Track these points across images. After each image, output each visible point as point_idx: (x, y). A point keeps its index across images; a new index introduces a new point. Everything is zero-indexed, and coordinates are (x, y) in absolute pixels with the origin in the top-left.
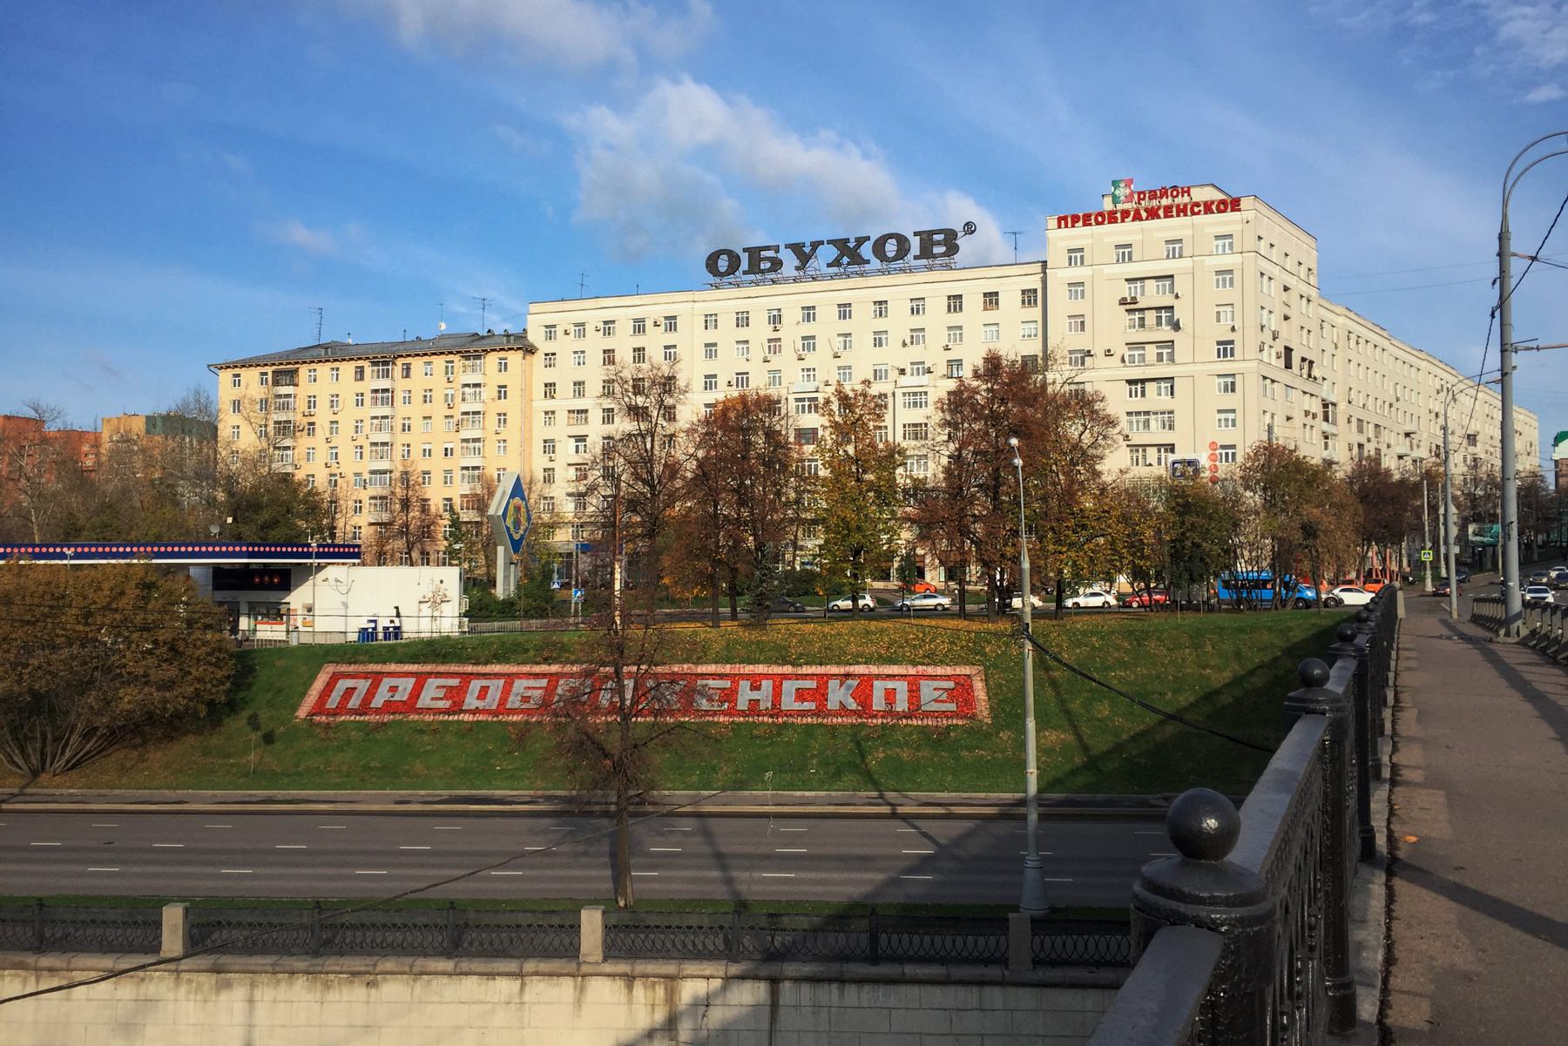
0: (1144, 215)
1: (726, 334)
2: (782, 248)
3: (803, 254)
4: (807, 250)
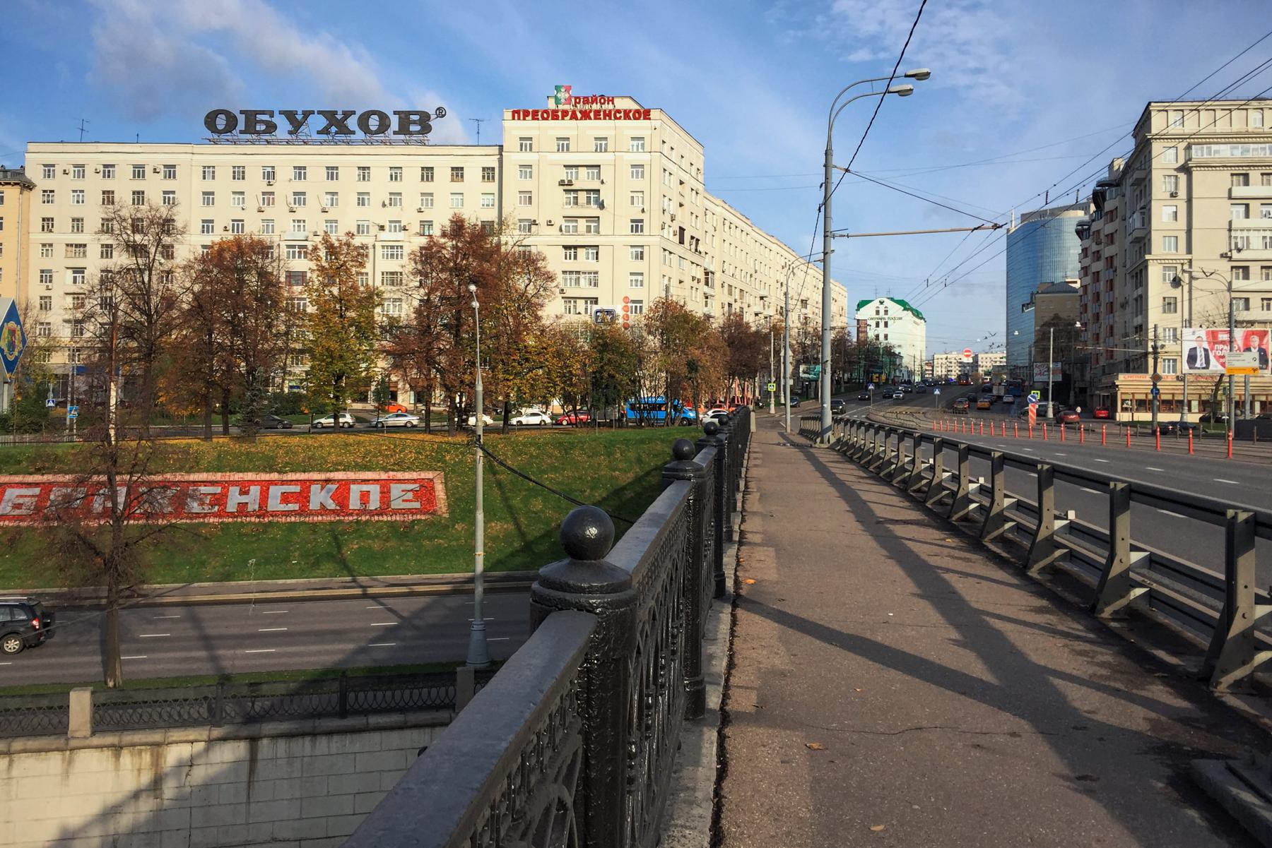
0: (579, 115)
1: (223, 185)
2: (276, 114)
4: (299, 117)
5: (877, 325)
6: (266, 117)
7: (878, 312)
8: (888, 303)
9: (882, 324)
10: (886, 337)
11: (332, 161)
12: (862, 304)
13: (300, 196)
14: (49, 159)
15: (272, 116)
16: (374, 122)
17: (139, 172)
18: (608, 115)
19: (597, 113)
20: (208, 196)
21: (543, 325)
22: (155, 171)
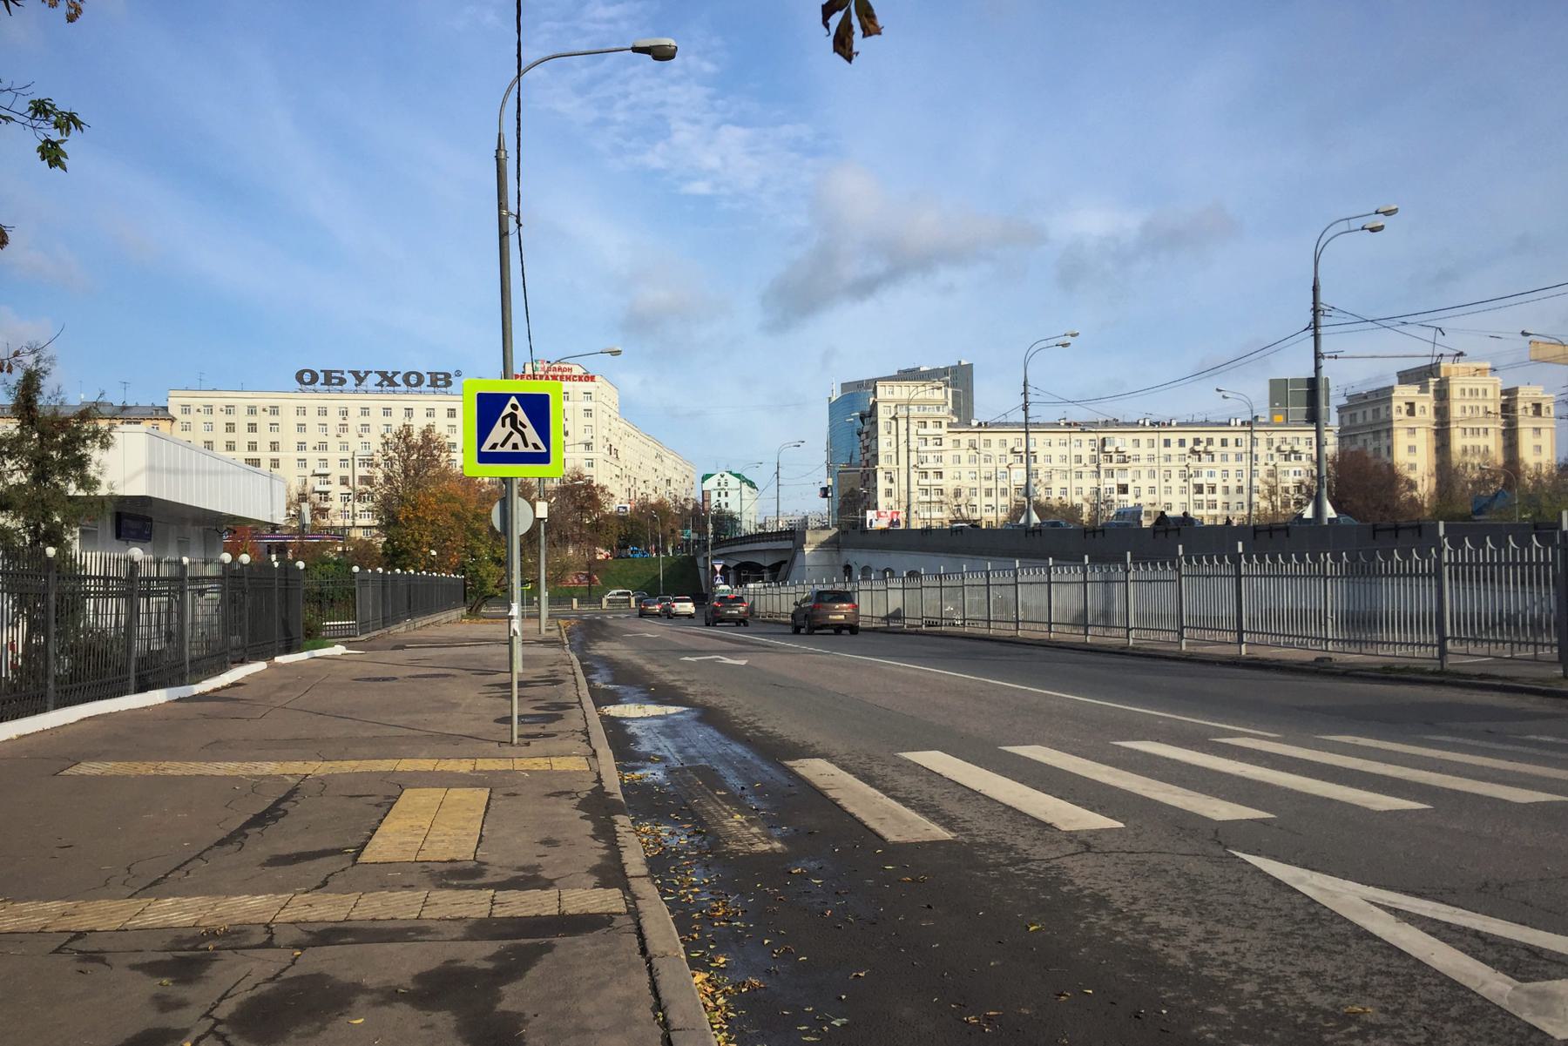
1: (312, 419)
2: (346, 373)
3: (360, 378)
4: (362, 375)
5: (719, 495)
6: (338, 375)
7: (719, 484)
8: (727, 476)
9: (723, 493)
10: (727, 504)
11: (387, 404)
12: (705, 478)
13: (366, 427)
14: (186, 401)
15: (343, 374)
16: (413, 379)
17: (252, 411)
18: (568, 378)
19: (562, 377)
20: (301, 427)
21: (70, 481)
22: (264, 410)
